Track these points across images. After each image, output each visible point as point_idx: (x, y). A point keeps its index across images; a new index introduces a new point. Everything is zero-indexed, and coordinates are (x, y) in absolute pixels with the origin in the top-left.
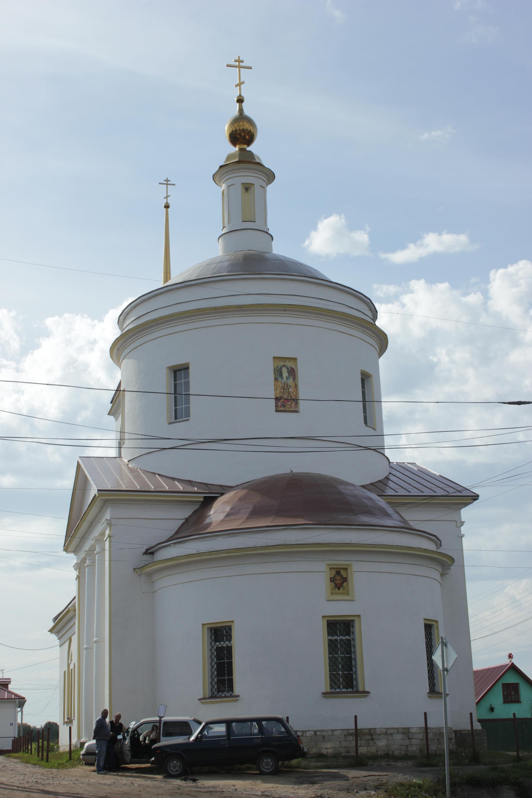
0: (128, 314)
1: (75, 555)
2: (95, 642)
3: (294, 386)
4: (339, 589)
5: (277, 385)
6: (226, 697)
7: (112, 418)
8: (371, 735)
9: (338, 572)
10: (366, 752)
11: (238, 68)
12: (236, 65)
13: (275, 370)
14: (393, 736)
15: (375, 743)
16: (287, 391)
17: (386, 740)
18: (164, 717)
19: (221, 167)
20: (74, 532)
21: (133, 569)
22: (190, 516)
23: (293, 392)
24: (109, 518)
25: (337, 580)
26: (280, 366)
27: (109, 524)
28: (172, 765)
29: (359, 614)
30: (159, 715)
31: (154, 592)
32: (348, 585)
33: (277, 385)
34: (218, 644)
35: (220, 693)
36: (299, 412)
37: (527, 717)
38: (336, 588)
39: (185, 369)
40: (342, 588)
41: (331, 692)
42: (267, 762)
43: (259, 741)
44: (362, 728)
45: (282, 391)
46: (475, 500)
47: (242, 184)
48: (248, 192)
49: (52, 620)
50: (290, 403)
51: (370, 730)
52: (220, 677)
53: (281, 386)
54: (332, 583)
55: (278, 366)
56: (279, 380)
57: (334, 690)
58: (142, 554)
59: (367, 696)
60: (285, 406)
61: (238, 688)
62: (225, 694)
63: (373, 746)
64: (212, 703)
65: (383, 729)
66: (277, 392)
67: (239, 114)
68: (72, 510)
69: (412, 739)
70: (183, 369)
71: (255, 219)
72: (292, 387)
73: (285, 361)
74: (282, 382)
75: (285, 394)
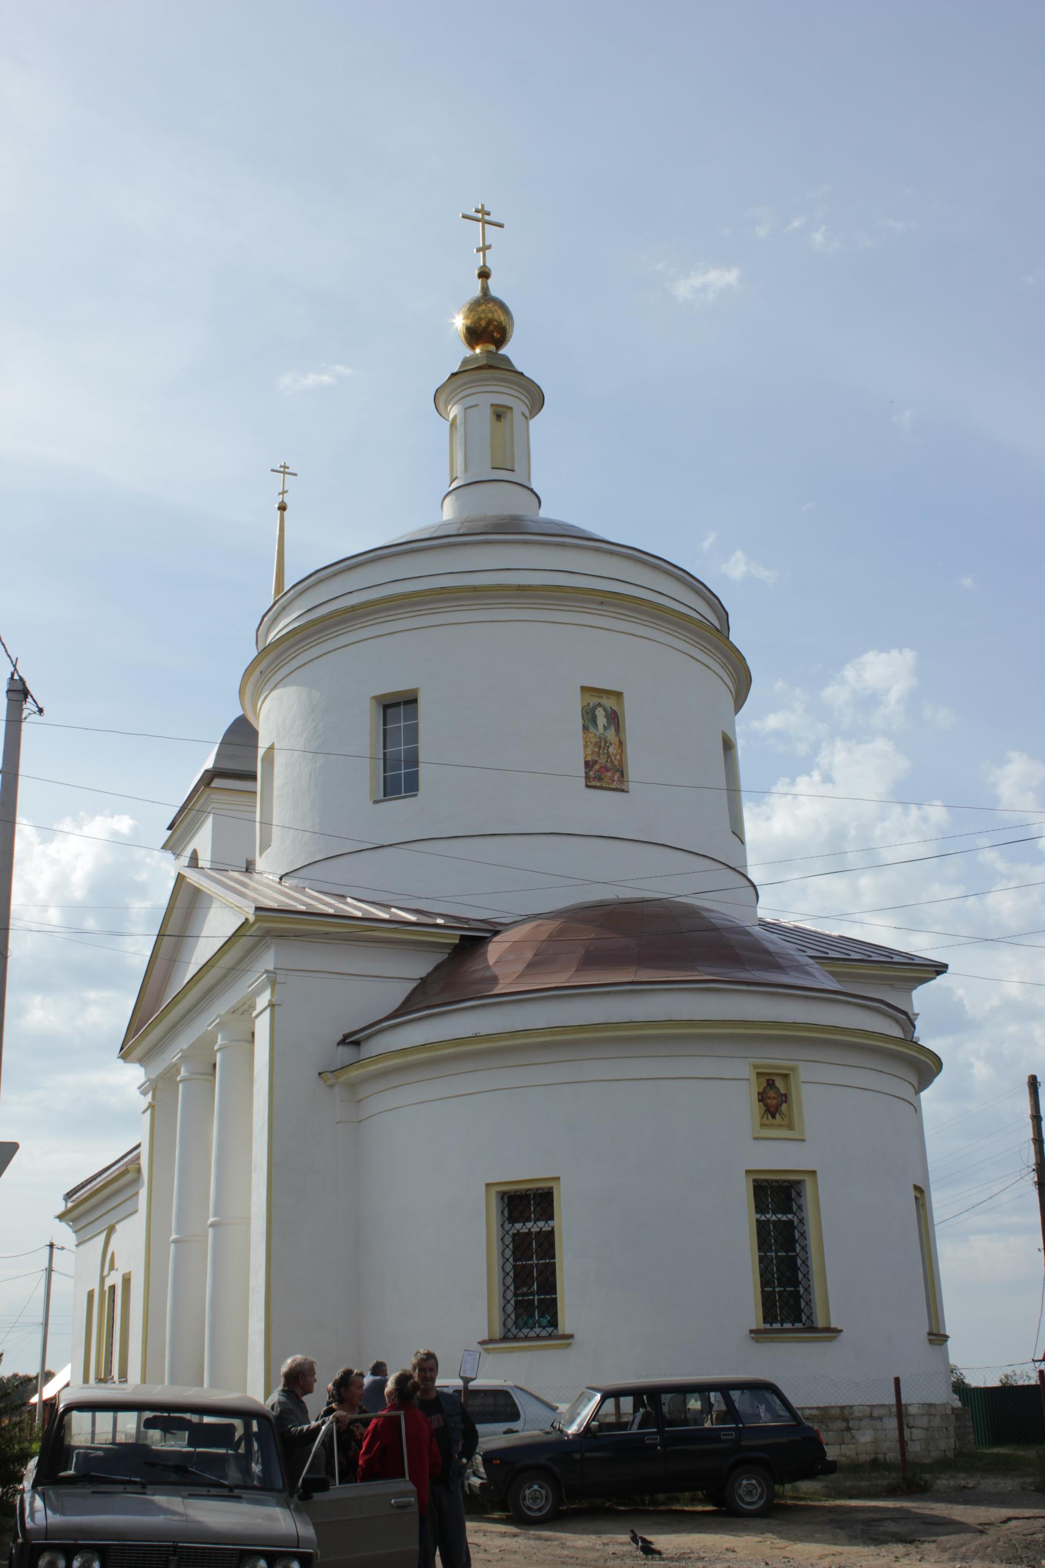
0: (284, 608)
1: (142, 1065)
2: (212, 1225)
3: (617, 743)
4: (774, 1117)
5: (588, 739)
6: (538, 1338)
7: (169, 855)
8: (845, 1420)
9: (771, 1082)
10: (837, 1456)
11: (481, 223)
12: (477, 218)
13: (584, 711)
14: (884, 1420)
15: (853, 1438)
16: (606, 751)
17: (872, 1432)
18: (475, 1379)
19: (453, 375)
20: (159, 1014)
21: (317, 1074)
22: (429, 975)
23: (616, 754)
24: (271, 968)
25: (769, 1098)
26: (593, 704)
27: (272, 979)
28: (530, 1494)
29: (814, 1170)
30: (462, 1375)
31: (360, 1122)
32: (790, 1109)
33: (588, 739)
34: (518, 1226)
35: (526, 1331)
36: (627, 792)
37: (970, 1383)
38: (768, 1115)
39: (406, 703)
40: (780, 1114)
41: (765, 1329)
42: (748, 1486)
43: (731, 1437)
44: (827, 1405)
45: (597, 750)
46: (939, 973)
47: (492, 405)
48: (500, 421)
49: (62, 1197)
50: (610, 775)
51: (842, 1408)
52: (523, 1299)
53: (594, 740)
54: (761, 1103)
55: (588, 704)
56: (590, 730)
57: (768, 1326)
58: (336, 1045)
59: (834, 1338)
60: (603, 779)
61: (568, 1319)
62: (538, 1333)
63: (849, 1443)
64: (512, 1350)
65: (865, 1408)
66: (587, 753)
67: (482, 294)
68: (150, 976)
69: (913, 1427)
70: (402, 704)
71: (513, 466)
72: (613, 746)
73: (602, 697)
74: (595, 735)
75: (601, 757)
